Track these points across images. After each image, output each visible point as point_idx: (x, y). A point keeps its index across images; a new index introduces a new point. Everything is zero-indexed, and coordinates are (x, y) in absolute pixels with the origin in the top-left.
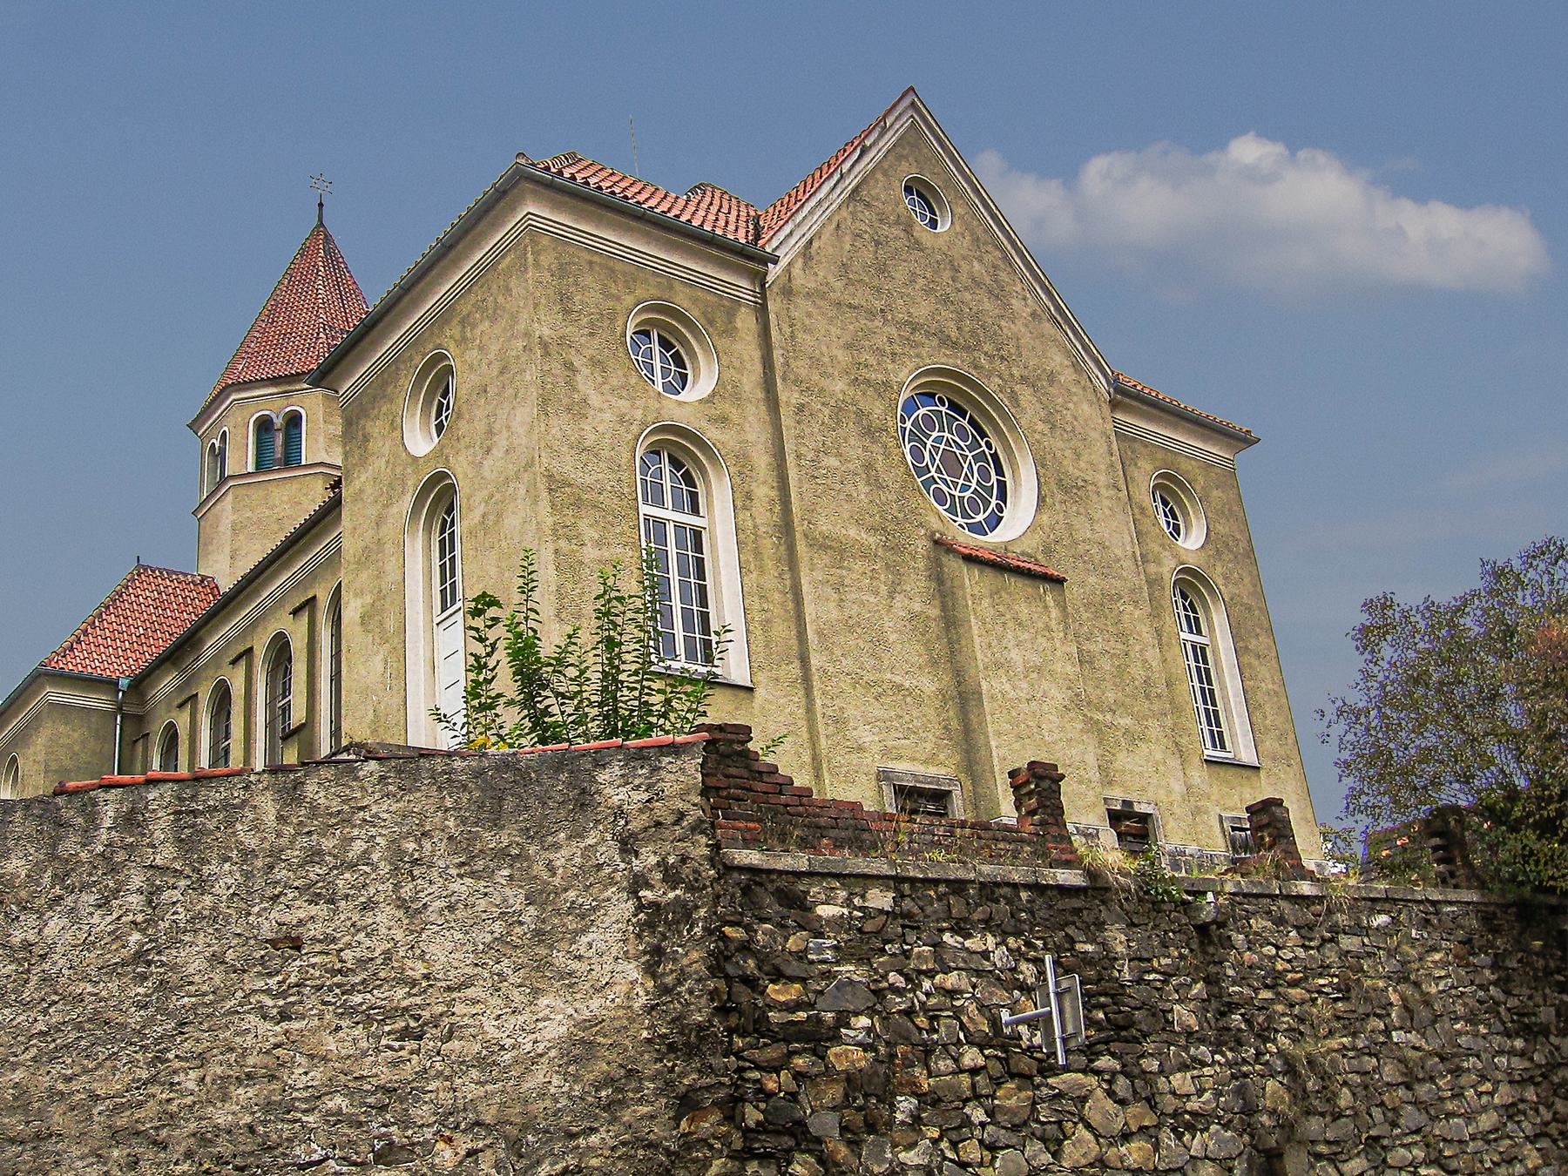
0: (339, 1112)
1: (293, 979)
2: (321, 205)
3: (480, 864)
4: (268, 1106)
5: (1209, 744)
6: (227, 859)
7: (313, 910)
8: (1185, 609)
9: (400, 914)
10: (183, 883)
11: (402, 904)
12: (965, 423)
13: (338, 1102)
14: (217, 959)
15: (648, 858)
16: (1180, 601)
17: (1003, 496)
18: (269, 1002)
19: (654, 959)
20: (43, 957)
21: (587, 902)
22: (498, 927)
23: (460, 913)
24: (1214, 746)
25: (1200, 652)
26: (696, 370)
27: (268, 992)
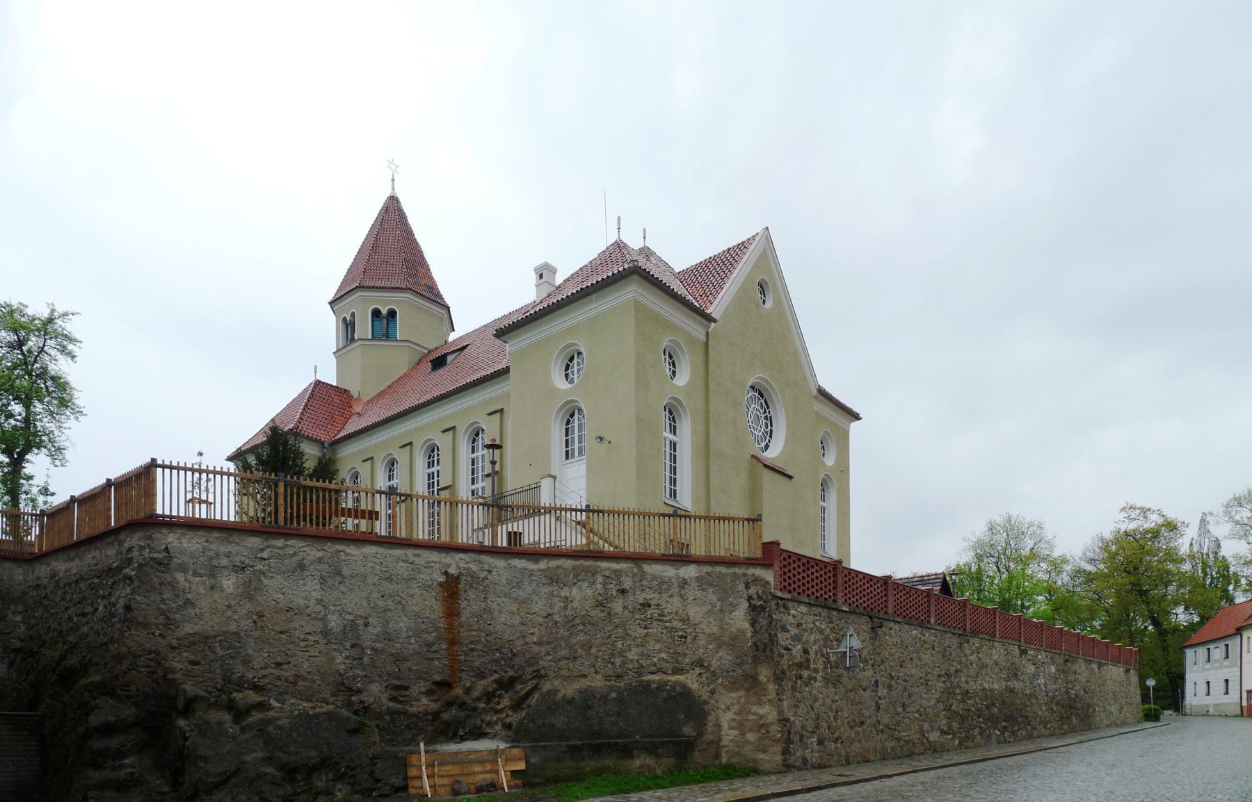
11: (681, 597)
13: (663, 655)
14: (625, 607)
15: (752, 591)
26: (680, 416)
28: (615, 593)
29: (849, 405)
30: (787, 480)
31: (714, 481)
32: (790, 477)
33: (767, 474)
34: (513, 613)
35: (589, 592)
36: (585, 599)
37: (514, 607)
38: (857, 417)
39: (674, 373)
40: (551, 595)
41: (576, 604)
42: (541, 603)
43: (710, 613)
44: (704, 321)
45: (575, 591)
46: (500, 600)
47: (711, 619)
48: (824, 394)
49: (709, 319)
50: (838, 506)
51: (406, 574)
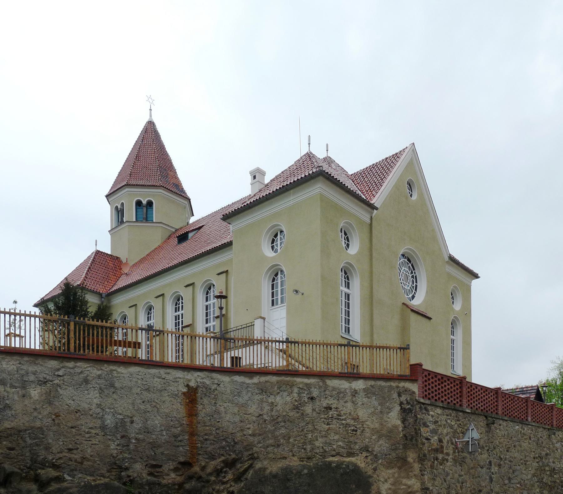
0: (340, 446)
1: (330, 416)
2: (151, 110)
3: (369, 395)
4: (326, 443)
5: (344, 331)
6: (315, 388)
7: (334, 401)
8: (345, 278)
9: (352, 404)
10: (306, 392)
11: (353, 402)
12: (410, 265)
14: (314, 410)
16: (344, 274)
17: (416, 290)
18: (325, 420)
19: (404, 421)
20: (276, 406)
21: (391, 406)
22: (373, 410)
23: (365, 406)
24: (346, 332)
25: (348, 296)
27: (325, 418)
28: (306, 400)
30: (428, 320)
32: (430, 319)
33: (413, 316)
34: (235, 414)
35: (288, 399)
36: (286, 404)
38: (476, 276)
39: (348, 245)
40: (262, 401)
41: (279, 407)
42: (254, 407)
43: (373, 413)
44: (369, 209)
45: (278, 398)
46: (225, 405)
47: (374, 418)
49: (373, 207)
50: (463, 339)
51: (159, 386)
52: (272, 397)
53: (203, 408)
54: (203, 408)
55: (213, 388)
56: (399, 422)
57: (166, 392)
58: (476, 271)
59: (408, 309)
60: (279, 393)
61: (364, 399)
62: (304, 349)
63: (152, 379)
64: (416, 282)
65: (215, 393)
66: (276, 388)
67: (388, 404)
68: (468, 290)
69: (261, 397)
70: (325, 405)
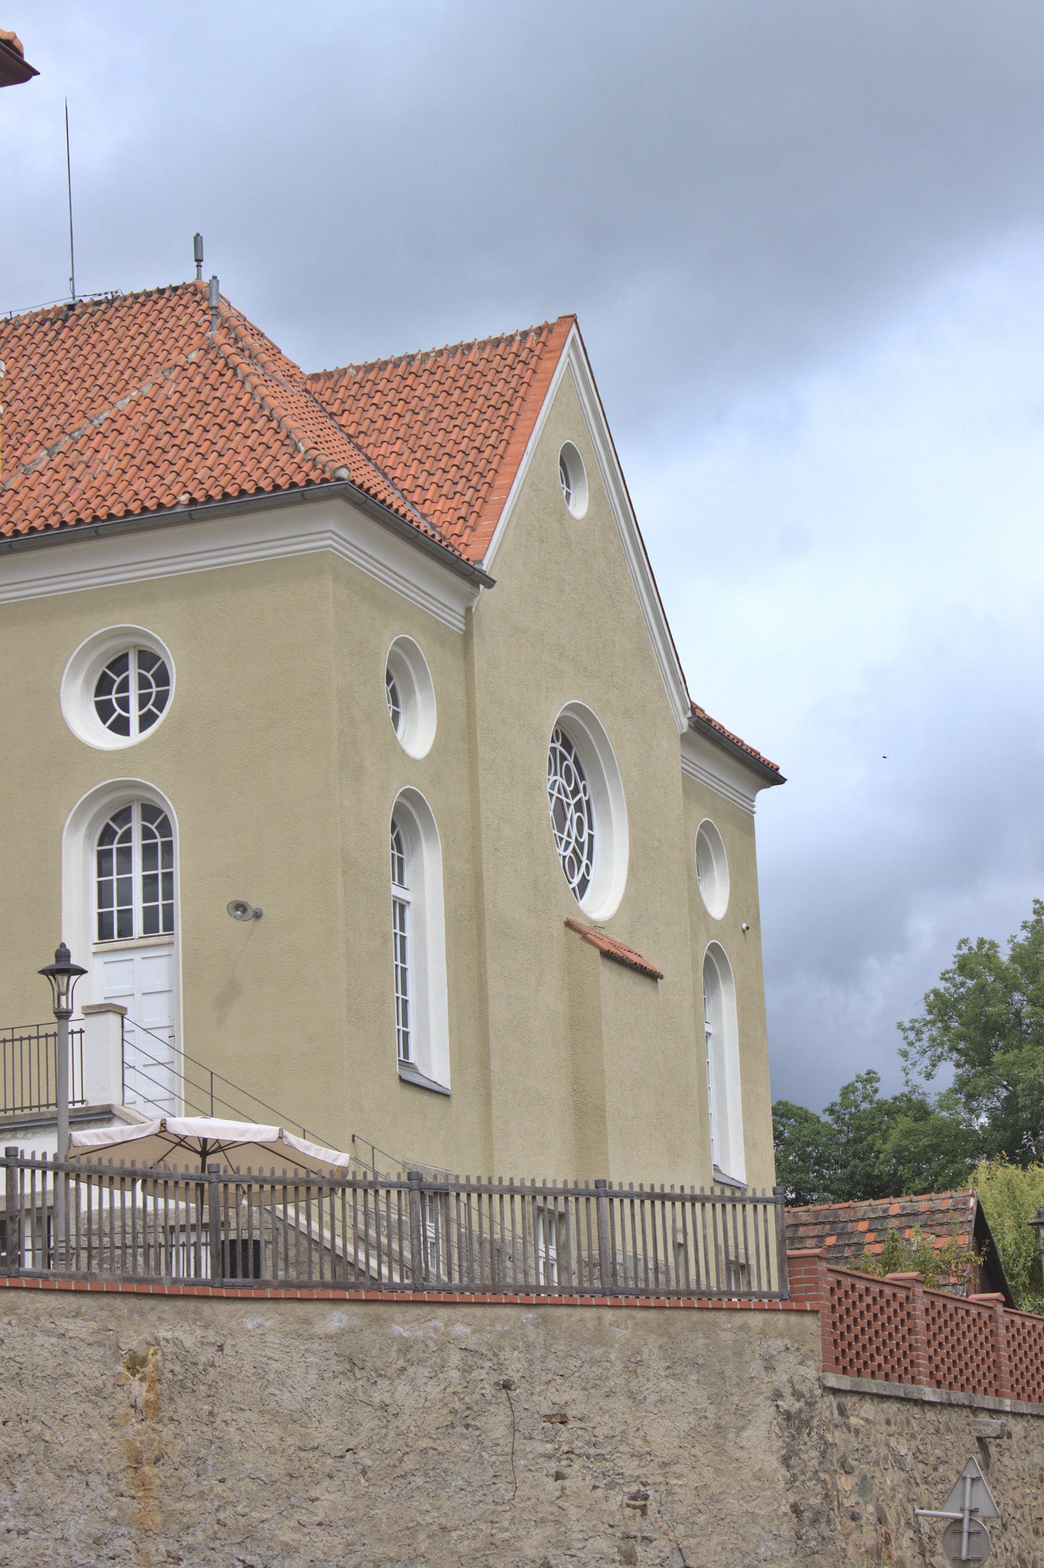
9: (630, 1402)
11: (631, 1395)
12: (570, 762)
17: (590, 857)
22: (693, 1419)
28: (489, 1390)
29: (752, 739)
30: (648, 982)
31: (497, 1010)
32: (653, 976)
33: (610, 977)
34: (271, 1450)
35: (433, 1390)
36: (426, 1410)
37: (272, 1435)
38: (771, 776)
39: (396, 716)
40: (351, 1399)
41: (405, 1422)
42: (330, 1422)
43: (694, 1434)
44: (466, 586)
45: (402, 1389)
46: (241, 1417)
47: (697, 1451)
48: (705, 731)
49: (475, 577)
50: (743, 1033)
51: (52, 1363)
52: (384, 1384)
53: (176, 1436)
54: (176, 1436)
55: (203, 1359)
56: (772, 1463)
57: (70, 1382)
58: (768, 754)
59: (586, 946)
60: (403, 1370)
61: (664, 1385)
62: (497, 1228)
63: (28, 1340)
64: (591, 827)
65: (209, 1379)
66: (394, 1354)
67: (735, 1399)
68: (746, 824)
69: (347, 1385)
70: (546, 1409)
